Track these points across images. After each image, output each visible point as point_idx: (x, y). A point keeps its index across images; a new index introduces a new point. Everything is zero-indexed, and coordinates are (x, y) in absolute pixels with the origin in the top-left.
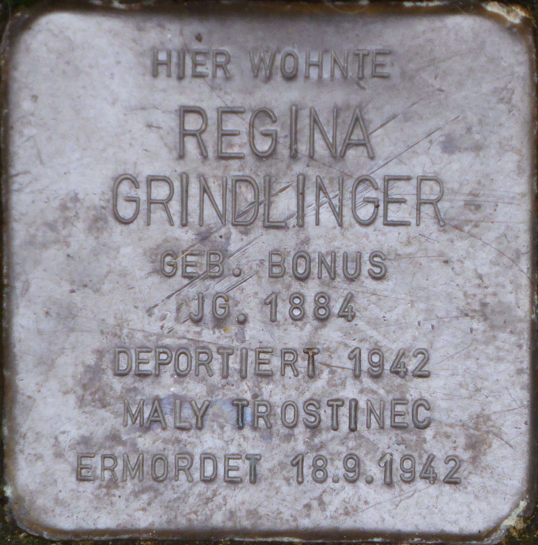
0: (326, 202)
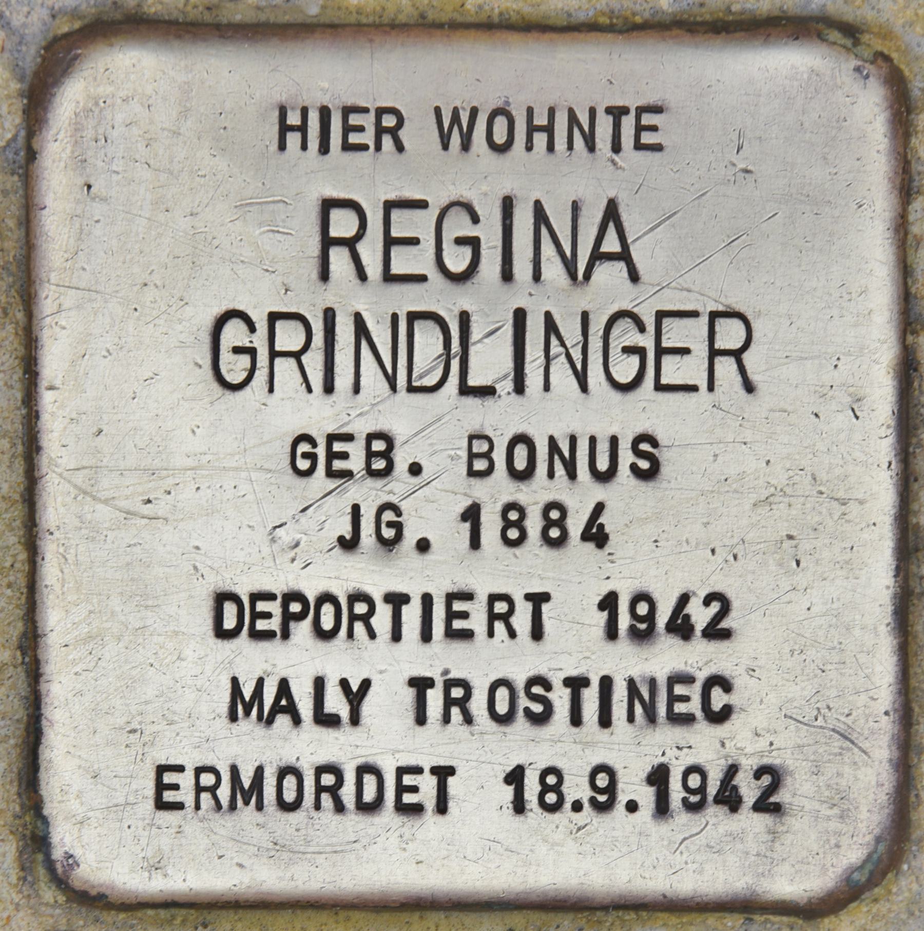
0: (561, 354)
